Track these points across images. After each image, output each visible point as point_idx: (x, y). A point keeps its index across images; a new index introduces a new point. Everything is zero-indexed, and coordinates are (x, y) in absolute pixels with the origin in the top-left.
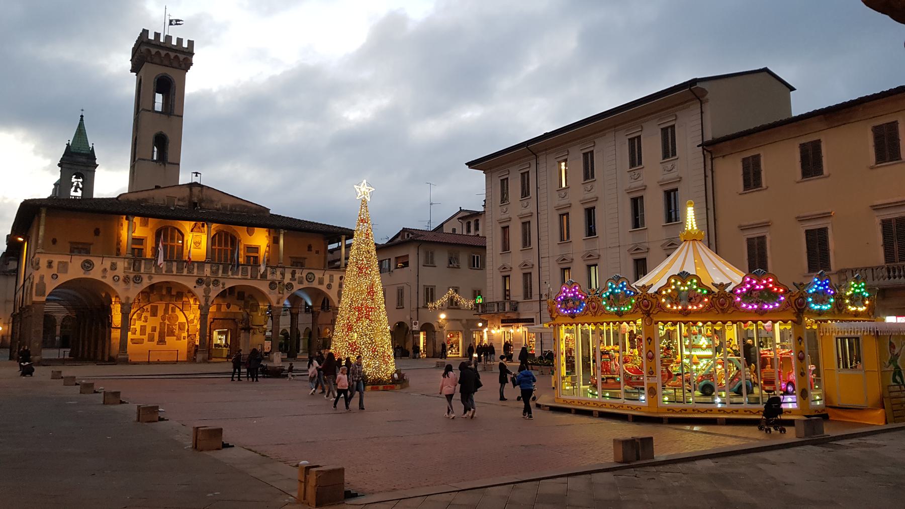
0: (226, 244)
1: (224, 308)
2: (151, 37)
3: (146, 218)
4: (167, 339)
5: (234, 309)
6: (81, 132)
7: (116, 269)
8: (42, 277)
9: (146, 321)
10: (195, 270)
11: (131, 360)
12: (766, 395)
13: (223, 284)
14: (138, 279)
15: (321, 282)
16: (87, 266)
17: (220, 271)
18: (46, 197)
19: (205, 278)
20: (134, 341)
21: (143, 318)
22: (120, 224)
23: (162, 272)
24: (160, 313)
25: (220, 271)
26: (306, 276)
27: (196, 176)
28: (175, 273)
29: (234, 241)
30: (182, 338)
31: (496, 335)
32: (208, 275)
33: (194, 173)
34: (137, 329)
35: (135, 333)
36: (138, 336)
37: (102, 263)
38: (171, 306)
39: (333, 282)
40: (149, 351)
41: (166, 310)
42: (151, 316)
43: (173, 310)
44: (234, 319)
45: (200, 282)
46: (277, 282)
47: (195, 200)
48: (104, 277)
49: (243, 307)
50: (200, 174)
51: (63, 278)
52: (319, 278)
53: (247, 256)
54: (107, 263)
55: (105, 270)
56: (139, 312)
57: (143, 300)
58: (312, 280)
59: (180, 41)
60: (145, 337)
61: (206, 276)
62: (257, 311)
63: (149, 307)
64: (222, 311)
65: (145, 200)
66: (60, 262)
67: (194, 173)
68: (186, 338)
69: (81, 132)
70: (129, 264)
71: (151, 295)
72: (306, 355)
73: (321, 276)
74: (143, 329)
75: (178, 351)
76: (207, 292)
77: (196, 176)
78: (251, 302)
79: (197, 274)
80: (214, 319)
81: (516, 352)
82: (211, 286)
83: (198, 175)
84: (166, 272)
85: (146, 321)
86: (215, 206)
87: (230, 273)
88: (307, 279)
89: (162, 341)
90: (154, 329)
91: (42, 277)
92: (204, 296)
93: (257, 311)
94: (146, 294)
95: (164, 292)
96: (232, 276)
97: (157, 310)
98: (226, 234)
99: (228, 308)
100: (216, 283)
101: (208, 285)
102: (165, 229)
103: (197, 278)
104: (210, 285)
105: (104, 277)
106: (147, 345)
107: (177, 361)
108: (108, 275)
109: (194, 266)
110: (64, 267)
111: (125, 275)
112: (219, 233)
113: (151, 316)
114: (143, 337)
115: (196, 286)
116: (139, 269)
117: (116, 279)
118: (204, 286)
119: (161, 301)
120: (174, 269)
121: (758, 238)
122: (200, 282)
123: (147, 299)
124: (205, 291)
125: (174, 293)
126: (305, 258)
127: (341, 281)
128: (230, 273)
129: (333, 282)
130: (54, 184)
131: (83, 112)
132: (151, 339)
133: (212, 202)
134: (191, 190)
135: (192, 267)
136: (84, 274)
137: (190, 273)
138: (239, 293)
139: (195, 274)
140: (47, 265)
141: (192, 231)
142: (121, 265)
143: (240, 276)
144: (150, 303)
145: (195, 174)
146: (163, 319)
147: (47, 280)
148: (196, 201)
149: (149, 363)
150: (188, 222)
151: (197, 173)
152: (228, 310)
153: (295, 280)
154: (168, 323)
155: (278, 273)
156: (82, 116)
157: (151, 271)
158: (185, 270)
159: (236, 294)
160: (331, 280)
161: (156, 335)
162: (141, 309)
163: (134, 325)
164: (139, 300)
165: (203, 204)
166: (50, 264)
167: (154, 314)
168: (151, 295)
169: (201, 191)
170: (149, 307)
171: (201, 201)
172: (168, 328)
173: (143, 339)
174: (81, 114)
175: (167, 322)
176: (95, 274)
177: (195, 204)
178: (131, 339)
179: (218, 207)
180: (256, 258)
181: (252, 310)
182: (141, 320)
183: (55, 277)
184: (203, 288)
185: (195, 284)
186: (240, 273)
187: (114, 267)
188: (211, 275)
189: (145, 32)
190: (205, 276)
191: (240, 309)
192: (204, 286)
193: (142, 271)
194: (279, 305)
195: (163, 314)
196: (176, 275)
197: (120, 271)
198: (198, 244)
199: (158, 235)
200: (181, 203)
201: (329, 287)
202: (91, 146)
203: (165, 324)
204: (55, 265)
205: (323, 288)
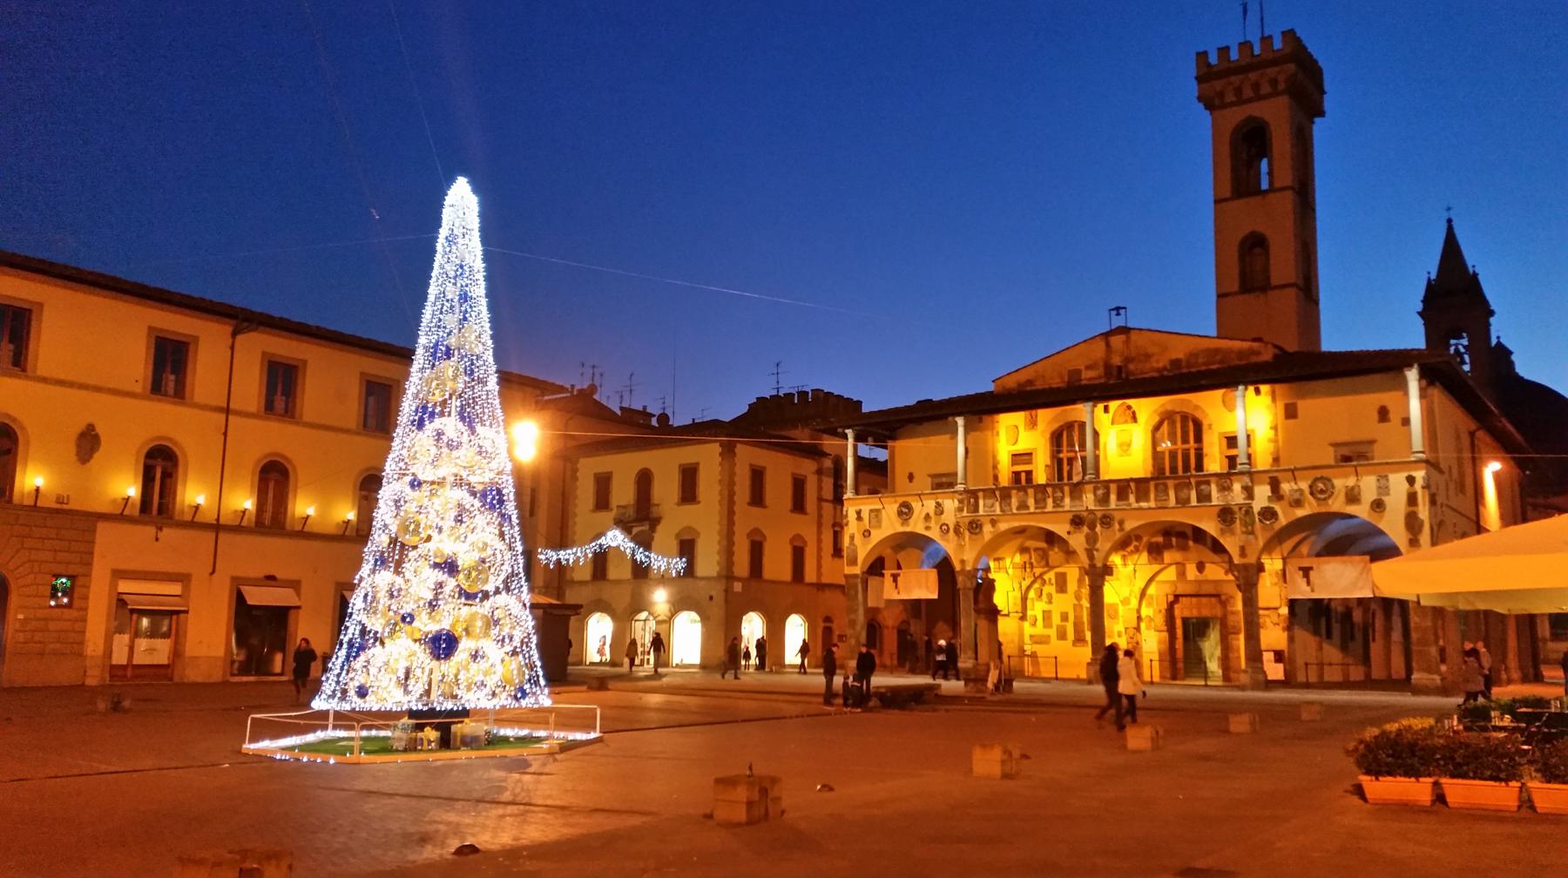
0: (1185, 440)
1: (1192, 572)
2: (1213, 59)
3: (1034, 412)
6: (1451, 250)
7: (942, 513)
8: (852, 538)
9: (1050, 602)
10: (1067, 500)
13: (1121, 523)
14: (975, 527)
15: (1353, 497)
17: (1113, 497)
18: (727, 420)
19: (1085, 514)
20: (1035, 639)
22: (995, 433)
23: (1011, 509)
25: (1113, 497)
26: (1311, 487)
27: (1118, 314)
28: (1032, 510)
29: (1195, 427)
30: (1116, 634)
32: (1092, 507)
33: (1113, 310)
34: (1038, 618)
35: (1034, 624)
36: (1039, 629)
37: (923, 505)
39: (1388, 494)
40: (1151, 661)
45: (1077, 521)
46: (1236, 509)
47: (1117, 360)
48: (928, 528)
51: (877, 536)
52: (1347, 487)
53: (1227, 457)
54: (930, 505)
55: (927, 517)
56: (1036, 585)
59: (1224, 51)
60: (1053, 632)
61: (1087, 510)
63: (1051, 576)
65: (1030, 382)
66: (871, 511)
67: (1113, 310)
68: (1124, 634)
69: (1451, 250)
70: (961, 501)
71: (1051, 553)
72: (1415, 679)
73: (1351, 482)
74: (1047, 616)
75: (1056, 658)
77: (1118, 314)
79: (1071, 507)
82: (1098, 529)
83: (1122, 312)
84: (1018, 509)
87: (1132, 498)
90: (1064, 617)
91: (852, 538)
94: (1040, 553)
96: (1135, 505)
98: (1185, 418)
100: (1107, 520)
101: (1092, 527)
102: (1069, 426)
103: (1070, 516)
104: (1096, 526)
105: (928, 528)
107: (1057, 678)
108: (932, 524)
109: (1063, 493)
112: (1167, 417)
115: (1072, 530)
117: (944, 529)
118: (1085, 529)
119: (1068, 563)
120: (1031, 502)
122: (1077, 521)
123: (1043, 563)
124: (1088, 538)
126: (1372, 442)
127: (1412, 490)
128: (1132, 498)
129: (1388, 494)
130: (757, 398)
131: (1452, 212)
132: (1062, 636)
133: (1148, 356)
134: (1108, 345)
135: (1059, 494)
137: (1058, 506)
139: (1067, 508)
140: (856, 516)
141: (1113, 423)
142: (950, 504)
143: (1152, 504)
145: (1114, 313)
147: (858, 540)
148: (1119, 364)
150: (1219, 393)
151: (1118, 309)
152: (1201, 577)
155: (1237, 487)
156: (1449, 221)
157: (994, 511)
158: (1050, 501)
160: (1384, 489)
162: (1039, 581)
163: (1033, 609)
164: (1031, 564)
165: (1132, 367)
169: (1127, 342)
170: (1051, 576)
171: (1128, 360)
173: (1049, 636)
174: (1447, 218)
176: (916, 526)
178: (1031, 636)
179: (1161, 365)
180: (1029, 473)
182: (1042, 600)
183: (867, 534)
184: (1085, 534)
185: (1067, 527)
186: (1152, 496)
187: (939, 509)
188: (1095, 506)
189: (1202, 56)
190: (1085, 508)
191: (1226, 573)
192: (1085, 529)
193: (981, 512)
195: (1076, 589)
196: (1034, 513)
197: (949, 517)
198: (1125, 447)
199: (1056, 439)
201: (1378, 505)
202: (1471, 270)
203: (1081, 606)
204: (865, 515)
205: (1362, 511)
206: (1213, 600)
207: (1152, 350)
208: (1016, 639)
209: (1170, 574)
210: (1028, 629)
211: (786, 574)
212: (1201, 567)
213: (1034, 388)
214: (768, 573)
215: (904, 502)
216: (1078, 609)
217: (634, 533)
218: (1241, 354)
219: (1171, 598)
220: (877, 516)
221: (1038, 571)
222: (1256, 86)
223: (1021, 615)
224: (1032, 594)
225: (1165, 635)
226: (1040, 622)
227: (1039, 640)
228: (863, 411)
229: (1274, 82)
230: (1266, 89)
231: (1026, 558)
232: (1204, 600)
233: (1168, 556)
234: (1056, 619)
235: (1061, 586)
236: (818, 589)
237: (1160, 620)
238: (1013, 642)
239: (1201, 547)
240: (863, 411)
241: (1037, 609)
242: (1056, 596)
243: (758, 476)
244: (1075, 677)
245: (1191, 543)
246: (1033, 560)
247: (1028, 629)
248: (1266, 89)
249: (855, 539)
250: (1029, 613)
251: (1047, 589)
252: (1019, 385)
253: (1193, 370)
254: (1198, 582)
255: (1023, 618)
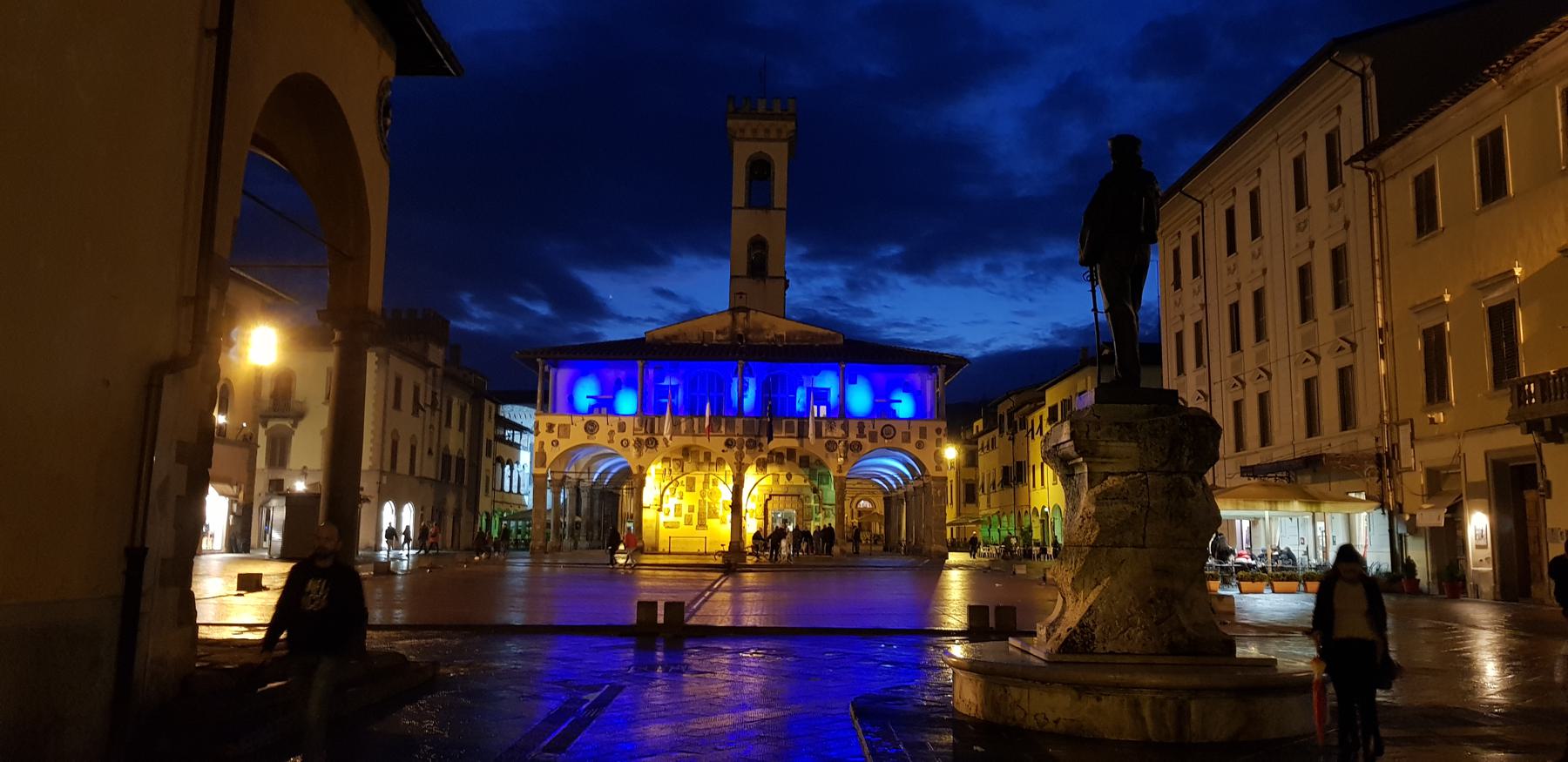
1: (783, 480)
4: (710, 522)
5: (798, 480)
9: (681, 498)
11: (1384, 513)
12: (1325, 552)
16: (591, 428)
20: (668, 524)
21: (677, 495)
24: (699, 486)
27: (741, 297)
31: (1058, 265)
35: (668, 514)
36: (671, 518)
38: (712, 477)
41: (706, 482)
42: (687, 491)
43: (715, 483)
44: (799, 496)
46: (837, 441)
47: (740, 330)
49: (808, 477)
50: (746, 294)
51: (565, 444)
55: (612, 432)
56: (672, 486)
57: (676, 470)
58: (893, 432)
60: (681, 520)
62: (828, 483)
64: (781, 483)
65: (675, 337)
74: (678, 508)
76: (740, 456)
78: (818, 471)
80: (770, 496)
81: (677, 495)
82: (745, 449)
83: (744, 296)
85: (681, 498)
86: (767, 337)
88: (882, 434)
89: (702, 525)
90: (691, 509)
92: (735, 463)
93: (828, 483)
94: (678, 462)
95: (702, 459)
97: (694, 484)
99: (789, 480)
105: (611, 441)
106: (684, 530)
110: (565, 431)
111: (635, 437)
113: (687, 491)
114: (678, 519)
115: (726, 449)
116: (652, 431)
118: (735, 449)
119: (698, 470)
121: (1435, 327)
125: (713, 459)
132: (689, 522)
133: (761, 330)
136: (588, 438)
138: (801, 458)
143: (783, 435)
144: (683, 475)
146: (703, 496)
148: (741, 333)
149: (670, 553)
151: (741, 293)
152: (788, 483)
153: (865, 436)
154: (710, 501)
159: (798, 460)
161: (695, 516)
162: (674, 483)
164: (670, 470)
165: (750, 336)
166: (550, 427)
167: (691, 489)
168: (685, 463)
169: (747, 318)
170: (684, 479)
171: (747, 331)
172: (709, 507)
173: (678, 522)
175: (707, 499)
177: (740, 337)
179: (770, 337)
181: (820, 483)
183: (555, 443)
191: (805, 481)
194: (840, 475)
200: (721, 337)
203: (705, 502)
206: (795, 498)
207: (766, 326)
208: (654, 525)
209: (768, 481)
210: (663, 518)
211: (407, 471)
212: (789, 477)
213: (678, 342)
214: (399, 470)
215: (590, 421)
216: (702, 503)
217: (269, 427)
218: (823, 337)
219: (767, 497)
220: (566, 429)
221: (674, 477)
222: (755, 131)
223: (658, 507)
224: (668, 492)
225: (762, 521)
226: (672, 512)
227: (675, 526)
228: (1141, 386)
229: (779, 131)
230: (773, 135)
231: (666, 465)
232: (788, 498)
233: (770, 469)
234: (685, 511)
235: (691, 489)
236: (421, 483)
237: (760, 512)
238: (651, 527)
239: (791, 463)
240: (1141, 386)
241: (670, 502)
242: (686, 495)
243: (399, 381)
244: (696, 551)
245: (785, 460)
246: (672, 468)
247: (663, 518)
248: (773, 135)
249: (545, 446)
250: (664, 506)
251: (679, 489)
252: (667, 338)
253: (793, 344)
254: (787, 487)
255: (660, 510)
